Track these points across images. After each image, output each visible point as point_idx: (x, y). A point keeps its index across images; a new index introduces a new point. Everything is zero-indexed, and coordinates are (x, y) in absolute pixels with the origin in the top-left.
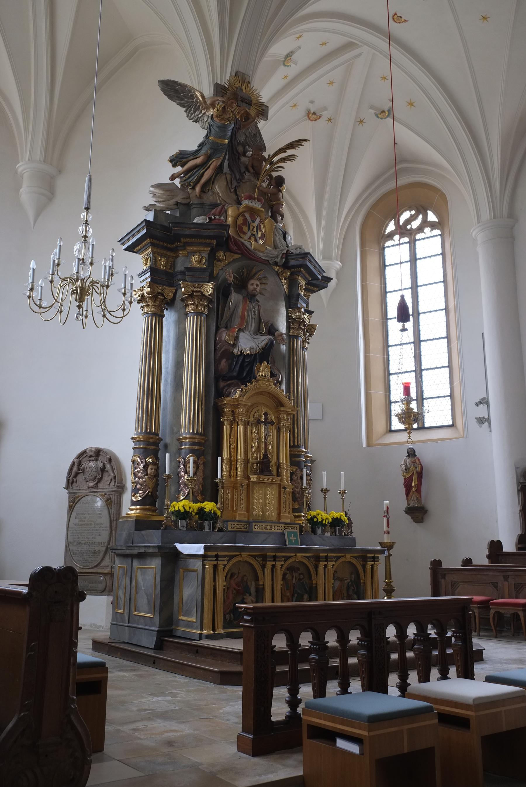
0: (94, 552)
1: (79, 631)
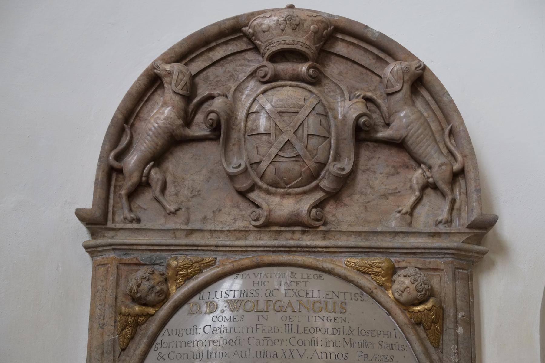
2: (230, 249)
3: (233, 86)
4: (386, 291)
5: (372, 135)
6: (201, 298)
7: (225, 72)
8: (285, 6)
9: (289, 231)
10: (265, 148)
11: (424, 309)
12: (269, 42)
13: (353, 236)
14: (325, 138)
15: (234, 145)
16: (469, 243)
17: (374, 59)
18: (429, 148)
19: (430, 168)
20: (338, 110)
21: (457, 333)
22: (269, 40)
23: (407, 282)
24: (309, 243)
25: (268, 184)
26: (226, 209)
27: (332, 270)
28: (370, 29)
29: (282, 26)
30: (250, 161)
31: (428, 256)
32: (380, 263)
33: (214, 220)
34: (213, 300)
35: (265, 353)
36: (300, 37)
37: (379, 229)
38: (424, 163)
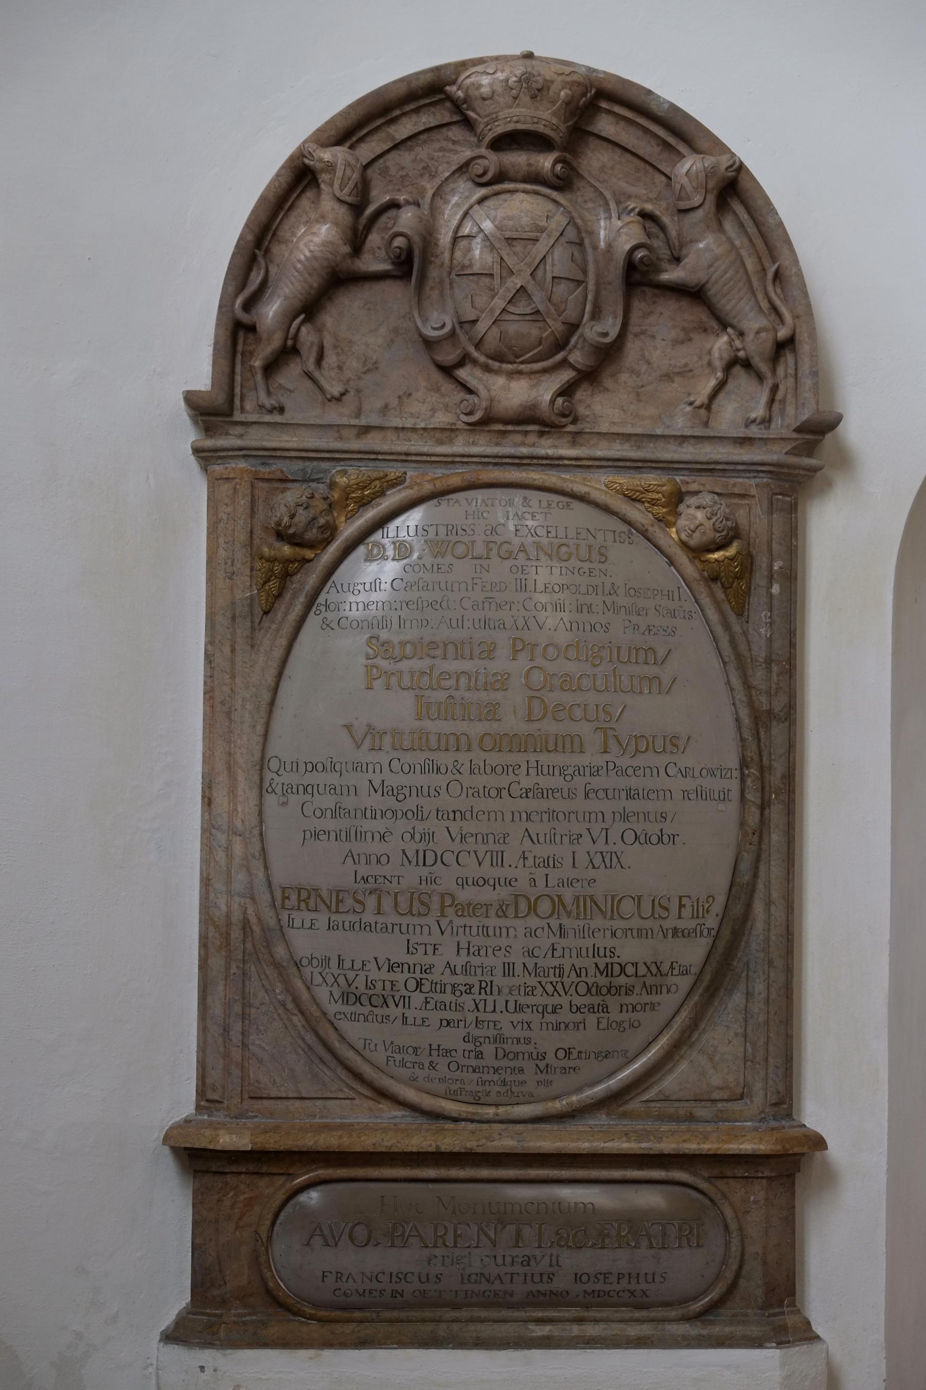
0: (603, 981)
1: (885, 1377)
2: (428, 459)
3: (428, 186)
4: (667, 529)
5: (652, 277)
6: (385, 536)
7: (414, 160)
8: (517, 52)
9: (519, 432)
10: (485, 298)
11: (723, 557)
12: (492, 118)
13: (618, 441)
14: (579, 283)
15: (432, 289)
16: (795, 455)
17: (658, 145)
18: (742, 303)
19: (741, 334)
20: (599, 234)
21: (771, 594)
22: (492, 114)
23: (700, 515)
24: (550, 452)
25: (488, 356)
26: (420, 394)
27: (587, 496)
28: (655, 97)
29: (514, 91)
30: (458, 317)
31: (732, 475)
32: (659, 486)
33: (401, 411)
34: (404, 539)
35: (487, 622)
36: (543, 111)
37: (659, 432)
38: (733, 327)
